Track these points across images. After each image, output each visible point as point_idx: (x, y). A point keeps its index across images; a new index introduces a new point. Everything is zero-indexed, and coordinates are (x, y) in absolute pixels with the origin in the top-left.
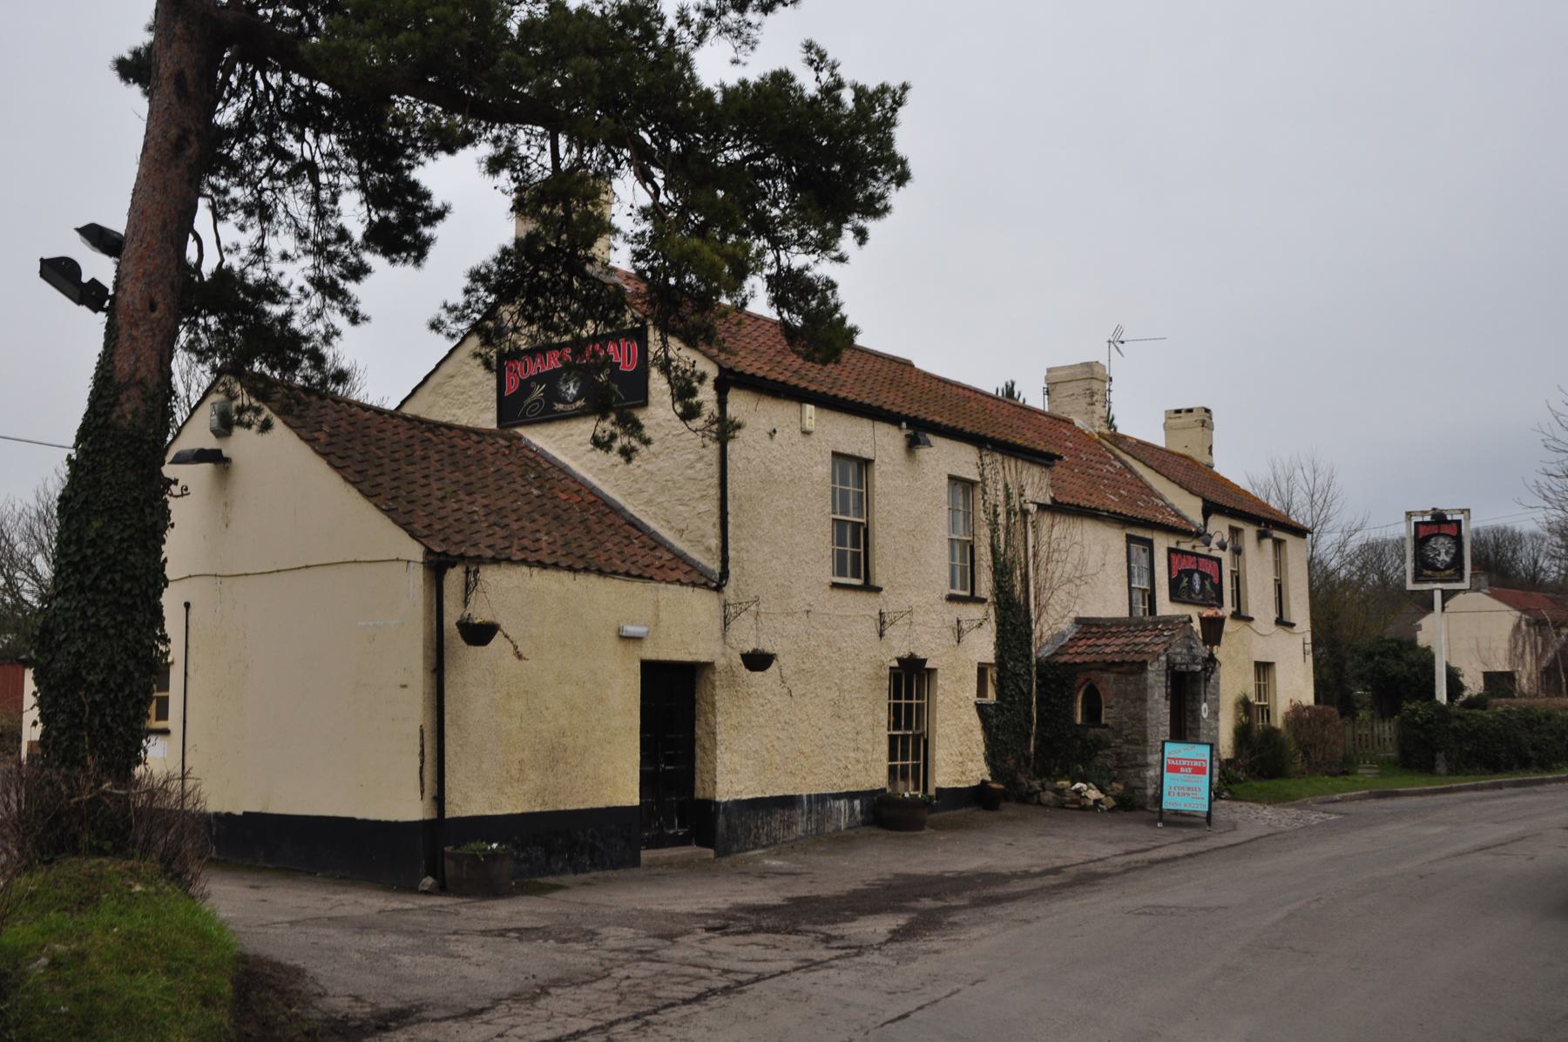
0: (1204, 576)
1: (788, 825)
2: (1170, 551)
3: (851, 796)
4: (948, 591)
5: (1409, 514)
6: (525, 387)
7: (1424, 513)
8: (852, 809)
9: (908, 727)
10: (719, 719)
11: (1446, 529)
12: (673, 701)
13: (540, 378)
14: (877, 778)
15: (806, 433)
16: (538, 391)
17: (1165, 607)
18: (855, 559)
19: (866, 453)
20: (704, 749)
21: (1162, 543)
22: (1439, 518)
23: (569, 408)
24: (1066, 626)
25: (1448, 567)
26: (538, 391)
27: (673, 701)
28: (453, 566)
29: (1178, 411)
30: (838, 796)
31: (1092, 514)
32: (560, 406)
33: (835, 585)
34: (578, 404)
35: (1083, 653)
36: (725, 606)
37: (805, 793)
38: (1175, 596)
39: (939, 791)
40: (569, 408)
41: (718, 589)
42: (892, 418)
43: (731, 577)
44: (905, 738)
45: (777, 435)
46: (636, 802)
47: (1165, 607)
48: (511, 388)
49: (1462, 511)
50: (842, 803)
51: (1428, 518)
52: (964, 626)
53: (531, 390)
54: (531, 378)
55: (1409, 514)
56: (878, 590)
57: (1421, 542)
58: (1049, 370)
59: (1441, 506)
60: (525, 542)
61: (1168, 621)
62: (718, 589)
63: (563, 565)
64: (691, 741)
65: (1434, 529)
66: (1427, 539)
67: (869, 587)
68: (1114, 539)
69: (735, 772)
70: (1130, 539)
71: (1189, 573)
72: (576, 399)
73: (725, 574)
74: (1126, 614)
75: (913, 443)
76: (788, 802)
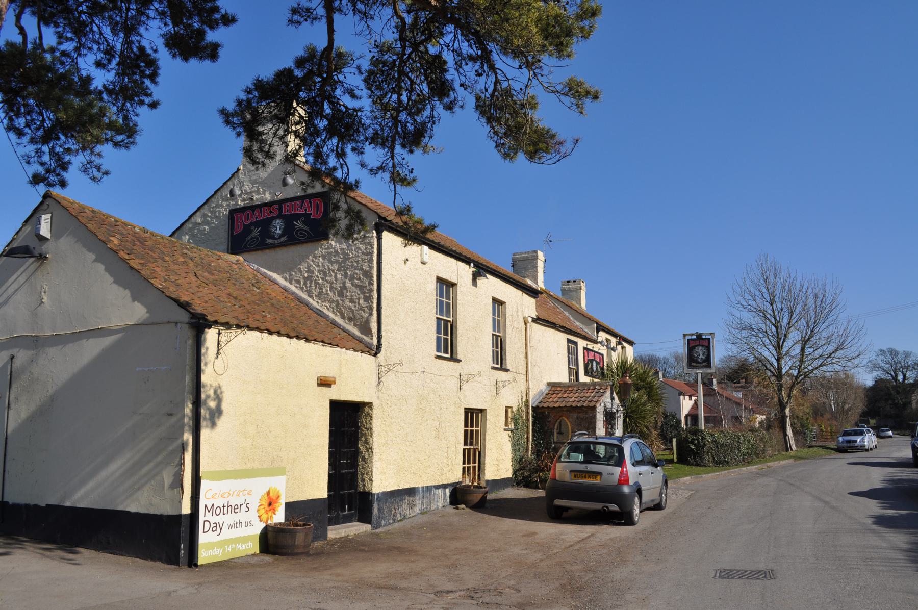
0: (598, 363)
1: (411, 506)
2: (585, 349)
3: (444, 486)
4: (492, 365)
5: (685, 335)
6: (247, 230)
7: (692, 335)
8: (445, 494)
9: (471, 444)
10: (375, 439)
11: (702, 342)
12: (348, 425)
13: (257, 224)
14: (455, 475)
15: (423, 263)
16: (256, 232)
17: (583, 378)
18: (447, 344)
19: (454, 280)
20: (364, 459)
21: (582, 343)
22: (699, 336)
23: (276, 242)
24: (543, 387)
25: (704, 361)
26: (256, 232)
27: (348, 425)
28: (210, 328)
29: (568, 282)
30: (437, 487)
31: (198, 385)
32: (270, 241)
33: (438, 357)
34: (282, 239)
35: (555, 402)
36: (379, 366)
37: (420, 486)
38: (586, 374)
39: (487, 481)
40: (276, 242)
41: (375, 355)
42: (467, 261)
43: (383, 349)
44: (469, 450)
45: (408, 263)
46: (325, 495)
47: (583, 378)
48: (238, 229)
49: (711, 334)
50: (440, 491)
51: (694, 337)
52: (500, 384)
53: (251, 231)
54: (252, 224)
55: (685, 335)
56: (459, 361)
57: (691, 349)
58: (514, 255)
59: (700, 331)
60: (258, 317)
61: (585, 384)
62: (375, 355)
63: (282, 332)
64: (357, 452)
65: (697, 343)
66: (694, 347)
67: (454, 359)
68: (562, 337)
69: (383, 475)
70: (569, 341)
71: (591, 361)
72: (281, 236)
73: (379, 345)
74: (567, 381)
75: (475, 276)
76: (410, 492)
